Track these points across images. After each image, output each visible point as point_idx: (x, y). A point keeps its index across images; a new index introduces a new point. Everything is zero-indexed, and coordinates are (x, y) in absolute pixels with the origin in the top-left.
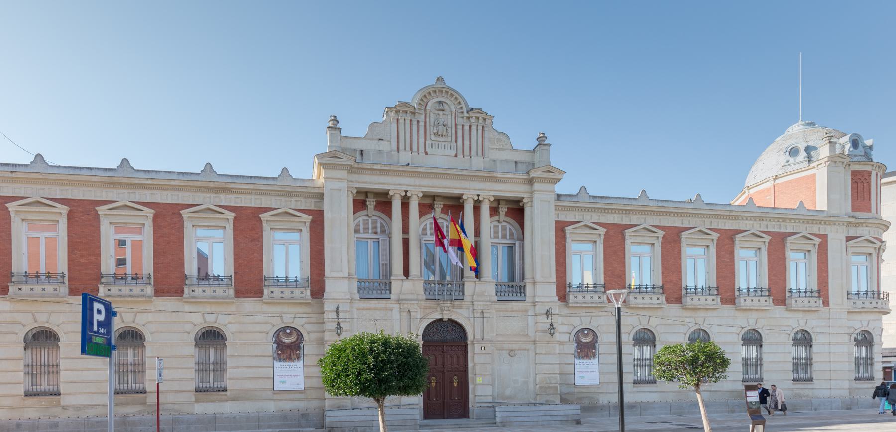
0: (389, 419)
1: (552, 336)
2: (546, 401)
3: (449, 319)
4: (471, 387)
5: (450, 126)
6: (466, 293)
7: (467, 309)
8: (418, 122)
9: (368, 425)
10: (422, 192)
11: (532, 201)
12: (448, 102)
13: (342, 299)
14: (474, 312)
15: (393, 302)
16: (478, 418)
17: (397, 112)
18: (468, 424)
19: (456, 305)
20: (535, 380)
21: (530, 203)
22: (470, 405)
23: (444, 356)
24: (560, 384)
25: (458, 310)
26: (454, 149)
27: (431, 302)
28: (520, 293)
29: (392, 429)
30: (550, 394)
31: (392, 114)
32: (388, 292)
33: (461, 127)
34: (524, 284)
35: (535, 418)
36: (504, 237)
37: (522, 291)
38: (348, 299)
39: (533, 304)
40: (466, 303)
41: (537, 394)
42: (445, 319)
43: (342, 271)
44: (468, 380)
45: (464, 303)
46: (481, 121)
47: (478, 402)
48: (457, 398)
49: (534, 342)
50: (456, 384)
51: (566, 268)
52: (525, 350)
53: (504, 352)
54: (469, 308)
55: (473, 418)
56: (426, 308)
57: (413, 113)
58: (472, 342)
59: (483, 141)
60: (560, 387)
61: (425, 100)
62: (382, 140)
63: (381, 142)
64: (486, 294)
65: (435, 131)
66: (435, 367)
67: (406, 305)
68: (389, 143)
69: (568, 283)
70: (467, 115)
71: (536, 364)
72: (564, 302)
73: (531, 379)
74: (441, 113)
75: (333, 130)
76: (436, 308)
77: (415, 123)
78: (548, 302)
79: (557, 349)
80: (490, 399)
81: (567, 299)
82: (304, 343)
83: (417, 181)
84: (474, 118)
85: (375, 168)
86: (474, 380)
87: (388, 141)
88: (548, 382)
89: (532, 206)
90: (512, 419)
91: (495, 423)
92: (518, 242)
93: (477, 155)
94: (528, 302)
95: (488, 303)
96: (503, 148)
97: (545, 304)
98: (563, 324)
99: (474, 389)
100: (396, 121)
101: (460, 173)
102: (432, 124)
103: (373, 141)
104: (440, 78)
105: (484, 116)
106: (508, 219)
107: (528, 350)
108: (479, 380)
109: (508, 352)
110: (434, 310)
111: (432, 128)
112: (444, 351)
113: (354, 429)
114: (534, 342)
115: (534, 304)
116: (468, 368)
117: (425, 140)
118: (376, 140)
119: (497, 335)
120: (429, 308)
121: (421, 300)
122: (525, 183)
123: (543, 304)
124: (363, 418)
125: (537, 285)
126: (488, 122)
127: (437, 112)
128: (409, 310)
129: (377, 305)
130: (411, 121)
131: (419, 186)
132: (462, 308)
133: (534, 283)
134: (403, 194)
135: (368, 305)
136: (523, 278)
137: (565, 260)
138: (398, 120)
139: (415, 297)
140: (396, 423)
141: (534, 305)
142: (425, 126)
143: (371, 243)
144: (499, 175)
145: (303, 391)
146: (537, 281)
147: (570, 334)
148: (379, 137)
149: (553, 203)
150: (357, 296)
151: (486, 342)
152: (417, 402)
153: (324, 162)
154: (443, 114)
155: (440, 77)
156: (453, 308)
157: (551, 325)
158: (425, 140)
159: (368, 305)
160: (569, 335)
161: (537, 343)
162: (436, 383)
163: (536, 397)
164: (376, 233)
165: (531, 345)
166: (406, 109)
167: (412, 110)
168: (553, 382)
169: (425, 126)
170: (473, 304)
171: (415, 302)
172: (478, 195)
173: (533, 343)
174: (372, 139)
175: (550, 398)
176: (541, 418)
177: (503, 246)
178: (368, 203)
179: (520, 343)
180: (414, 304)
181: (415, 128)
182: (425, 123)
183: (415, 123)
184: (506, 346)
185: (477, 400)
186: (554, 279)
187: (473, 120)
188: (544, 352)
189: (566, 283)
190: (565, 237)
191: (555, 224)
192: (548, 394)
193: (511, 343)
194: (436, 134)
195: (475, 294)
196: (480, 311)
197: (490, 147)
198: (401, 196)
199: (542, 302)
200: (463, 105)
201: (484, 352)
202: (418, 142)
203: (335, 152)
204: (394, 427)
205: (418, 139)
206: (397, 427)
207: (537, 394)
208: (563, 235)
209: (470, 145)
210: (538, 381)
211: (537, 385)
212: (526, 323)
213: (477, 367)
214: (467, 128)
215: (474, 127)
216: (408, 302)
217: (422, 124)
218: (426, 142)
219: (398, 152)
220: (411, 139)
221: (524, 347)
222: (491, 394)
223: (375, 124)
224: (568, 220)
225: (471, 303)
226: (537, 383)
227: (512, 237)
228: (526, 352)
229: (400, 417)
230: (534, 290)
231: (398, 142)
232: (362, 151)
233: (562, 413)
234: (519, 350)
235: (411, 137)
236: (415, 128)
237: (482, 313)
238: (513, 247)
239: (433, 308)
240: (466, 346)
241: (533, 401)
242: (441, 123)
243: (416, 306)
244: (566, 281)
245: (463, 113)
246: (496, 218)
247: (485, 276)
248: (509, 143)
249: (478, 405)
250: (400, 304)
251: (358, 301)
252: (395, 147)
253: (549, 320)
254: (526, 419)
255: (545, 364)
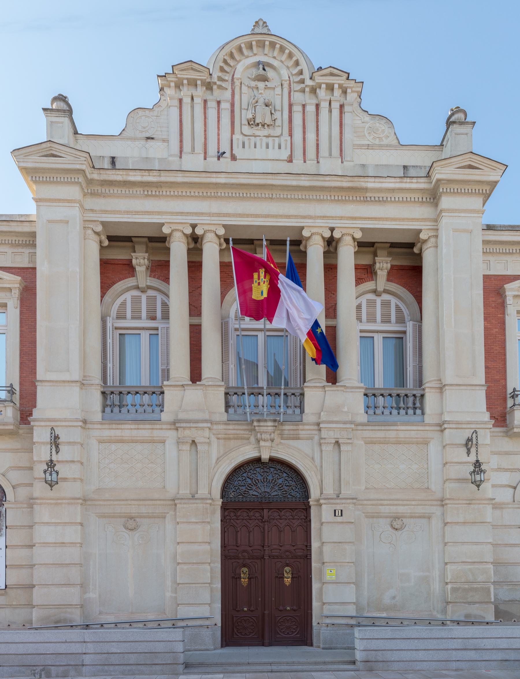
0: (119, 651)
1: (478, 486)
2: (467, 616)
3: (272, 460)
4: (315, 586)
5: (278, 107)
6: (307, 410)
7: (308, 439)
8: (219, 103)
9: (72, 663)
10: (224, 226)
11: (437, 237)
12: (275, 63)
13: (65, 420)
14: (320, 444)
15: (164, 427)
16: (327, 646)
17: (178, 86)
18: (293, 663)
19: (286, 432)
20: (443, 574)
21: (433, 240)
22: (314, 623)
23: (264, 528)
24: (494, 583)
25: (291, 442)
26: (286, 149)
27: (237, 427)
28: (415, 408)
29: (123, 673)
30: (475, 603)
31: (170, 92)
32: (298, 411)
33: (300, 108)
34: (422, 392)
35: (442, 656)
36: (386, 320)
37: (418, 405)
38: (77, 420)
39: (438, 428)
40: (307, 427)
41: (448, 603)
42: (265, 456)
43: (68, 371)
44: (311, 574)
45: (301, 427)
46: (337, 92)
47: (327, 617)
48: (245, 609)
49: (442, 502)
50: (288, 581)
51: (505, 364)
52: (424, 517)
53: (382, 521)
54: (312, 439)
55: (319, 647)
56: (230, 439)
57: (209, 86)
58: (318, 500)
59: (341, 133)
60: (494, 589)
61: (232, 63)
62: (153, 138)
63: (150, 142)
64: (346, 409)
65: (250, 116)
66: (249, 549)
67: (187, 432)
68: (166, 144)
69: (510, 390)
70: (309, 82)
71: (446, 544)
72: (503, 426)
73: (436, 573)
74: (261, 85)
75: (55, 114)
76: (248, 439)
77: (212, 104)
78: (469, 423)
79: (489, 514)
80: (352, 611)
81: (508, 422)
82: (6, 506)
83: (215, 206)
84: (323, 86)
85: (132, 178)
86: (321, 572)
87: (164, 141)
88: (471, 578)
89: (436, 247)
90: (389, 656)
91: (354, 663)
92: (411, 323)
93: (330, 155)
94: (429, 425)
95: (348, 426)
96: (382, 143)
97: (464, 426)
98: (499, 469)
99: (321, 590)
100: (177, 103)
101: (294, 183)
102: (244, 106)
103: (137, 143)
104: (261, 23)
105: (342, 80)
106: (394, 287)
107: (429, 518)
108: (330, 574)
109: (389, 520)
110: (245, 441)
111: (244, 112)
112: (266, 518)
113: (43, 670)
114: (442, 502)
115: (441, 427)
116: (311, 550)
117: (233, 132)
118: (141, 139)
119: (367, 488)
120: (235, 439)
121: (218, 423)
122: (422, 202)
123: (460, 426)
124: (62, 648)
125: (448, 392)
126: (351, 96)
127: (253, 84)
128: (193, 441)
129: (135, 433)
130: (205, 101)
131: (219, 215)
132: (298, 439)
133: (441, 389)
134: (189, 231)
135: (118, 433)
136: (420, 382)
137: (504, 348)
138: (181, 101)
139: (207, 416)
140: (133, 659)
141: (442, 431)
142: (232, 111)
143: (145, 335)
144: (371, 184)
145: (3, 592)
146: (446, 383)
147: (515, 488)
148: (148, 135)
149: (479, 236)
150: (98, 417)
151: (344, 501)
152: (207, 615)
153: (30, 165)
154: (266, 88)
155: (261, 19)
156: (282, 438)
157: (477, 464)
158: (233, 132)
159: (118, 433)
160: (511, 490)
161: (447, 502)
162: (249, 578)
163: (176, 589)
164: (154, 318)
165: (435, 507)
166: (193, 75)
167: (205, 76)
168: (481, 578)
169: (232, 111)
170: (320, 430)
171: (205, 425)
172: (332, 230)
173: (439, 503)
174: (134, 139)
175: (475, 610)
176: (455, 655)
177: (383, 337)
178: (134, 262)
179: (413, 503)
180: (203, 428)
181: (212, 113)
182: (233, 105)
183: (212, 104)
184: (385, 510)
185: (326, 612)
186: (481, 378)
187: (322, 93)
188: (461, 520)
189: (506, 392)
190: (503, 305)
191: (484, 282)
192: (469, 603)
193: (395, 502)
194: (252, 123)
195: (324, 410)
196: (333, 441)
197: (355, 143)
198: (184, 234)
199: (458, 423)
200: (303, 65)
201: (339, 519)
202: (219, 140)
203: (48, 144)
204: (128, 668)
205: (219, 135)
206: (134, 667)
207: (448, 603)
208: (500, 301)
209: (317, 140)
210: (449, 577)
211: (447, 583)
212: (426, 466)
213: (326, 549)
214: (311, 109)
215: (324, 105)
216: (192, 425)
217: (225, 106)
218: (234, 137)
219: (181, 157)
220: (205, 135)
221: (420, 510)
222: (355, 601)
223: (140, 112)
224: (509, 273)
225: (316, 427)
226: (449, 581)
227: (401, 320)
228: (425, 521)
229: (141, 647)
230: (442, 402)
231: (181, 141)
232: (113, 158)
233: (503, 644)
234: (411, 517)
235: (205, 131)
236: (212, 113)
237: (336, 447)
238: (402, 338)
239: (242, 438)
240: (307, 509)
241: (440, 616)
242: (261, 101)
243: (207, 433)
244: (505, 387)
245: (302, 81)
246: (369, 285)
247: (343, 378)
248: (393, 134)
249: (328, 621)
250: (177, 429)
251: (99, 426)
252: (177, 151)
253: (472, 458)
254: (421, 655)
255: (463, 543)
